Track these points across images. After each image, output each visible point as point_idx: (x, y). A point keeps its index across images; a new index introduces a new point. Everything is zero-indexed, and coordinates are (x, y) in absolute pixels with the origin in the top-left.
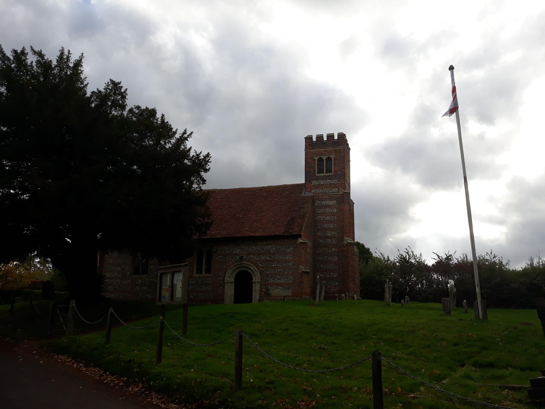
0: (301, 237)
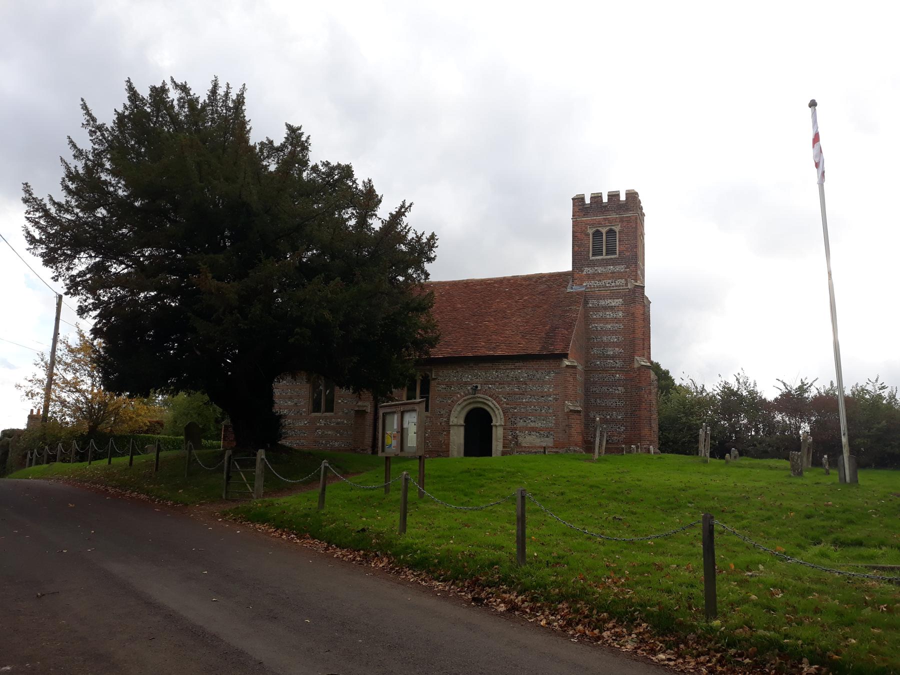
0: (567, 358)
